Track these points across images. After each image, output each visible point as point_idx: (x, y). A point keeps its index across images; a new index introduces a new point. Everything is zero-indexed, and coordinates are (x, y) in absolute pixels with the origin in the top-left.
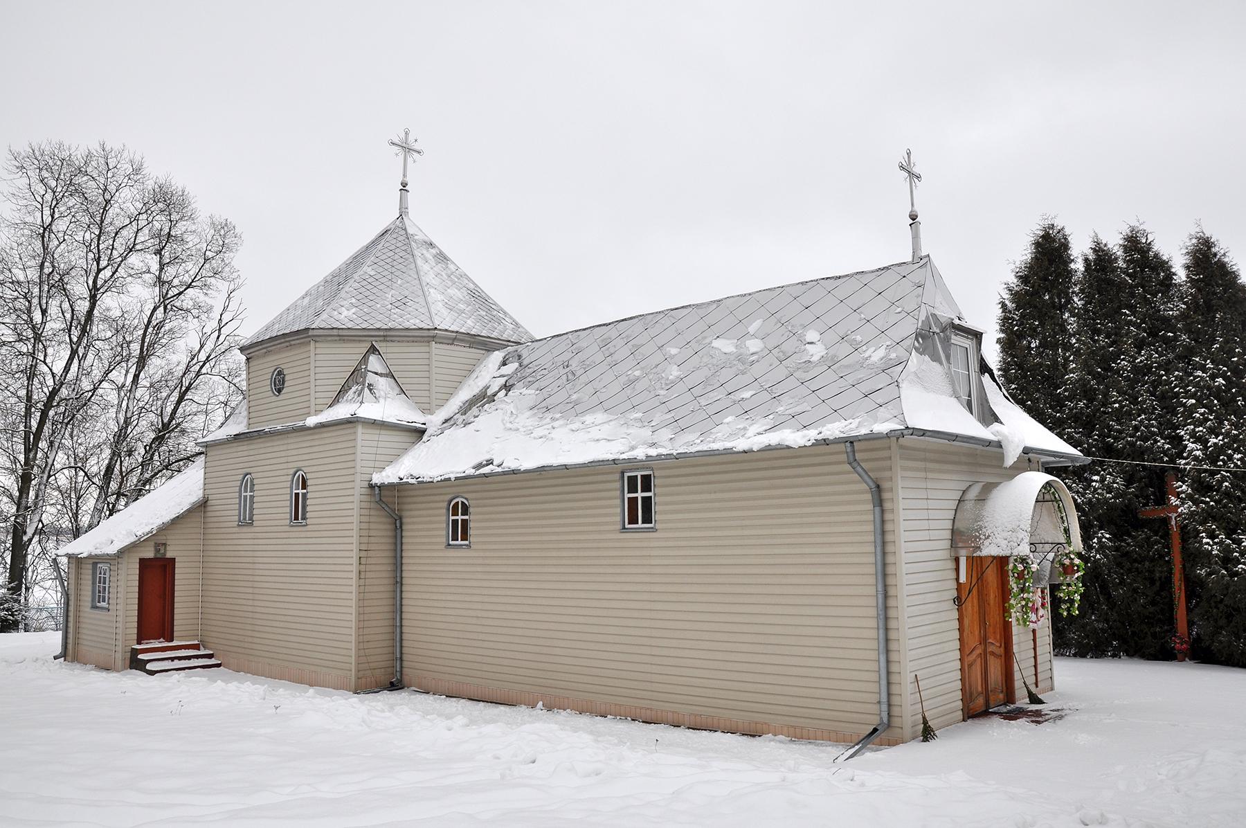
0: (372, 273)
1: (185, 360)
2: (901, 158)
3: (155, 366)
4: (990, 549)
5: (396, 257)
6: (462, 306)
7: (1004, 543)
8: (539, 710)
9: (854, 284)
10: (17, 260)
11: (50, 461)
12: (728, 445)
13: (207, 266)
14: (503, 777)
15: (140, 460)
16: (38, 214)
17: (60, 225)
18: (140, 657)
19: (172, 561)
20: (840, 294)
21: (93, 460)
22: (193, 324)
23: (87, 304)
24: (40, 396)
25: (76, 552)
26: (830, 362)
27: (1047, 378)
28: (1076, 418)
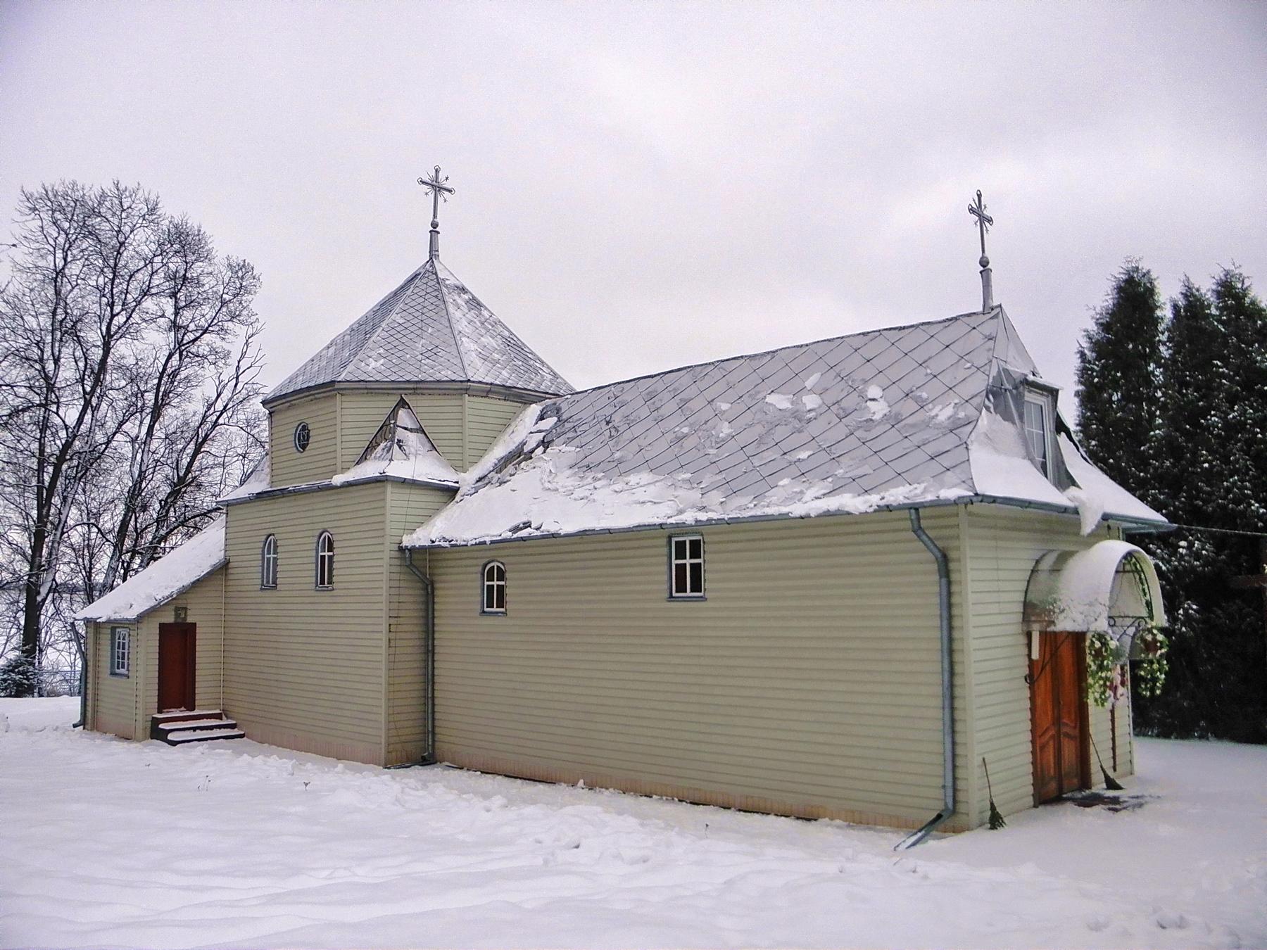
0: (401, 321)
1: (201, 410)
2: (971, 199)
3: (171, 415)
4: (1064, 624)
5: (427, 303)
6: (497, 356)
7: (1080, 618)
8: (580, 791)
9: (920, 336)
10: (29, 306)
11: (63, 517)
12: (784, 510)
13: (224, 309)
14: (546, 862)
15: (155, 516)
16: (51, 258)
17: (74, 269)
18: (161, 726)
20: (906, 345)
21: (106, 517)
22: (210, 371)
23: (101, 352)
24: (53, 447)
25: (95, 616)
26: (894, 420)
27: (1128, 434)
28: (1161, 479)
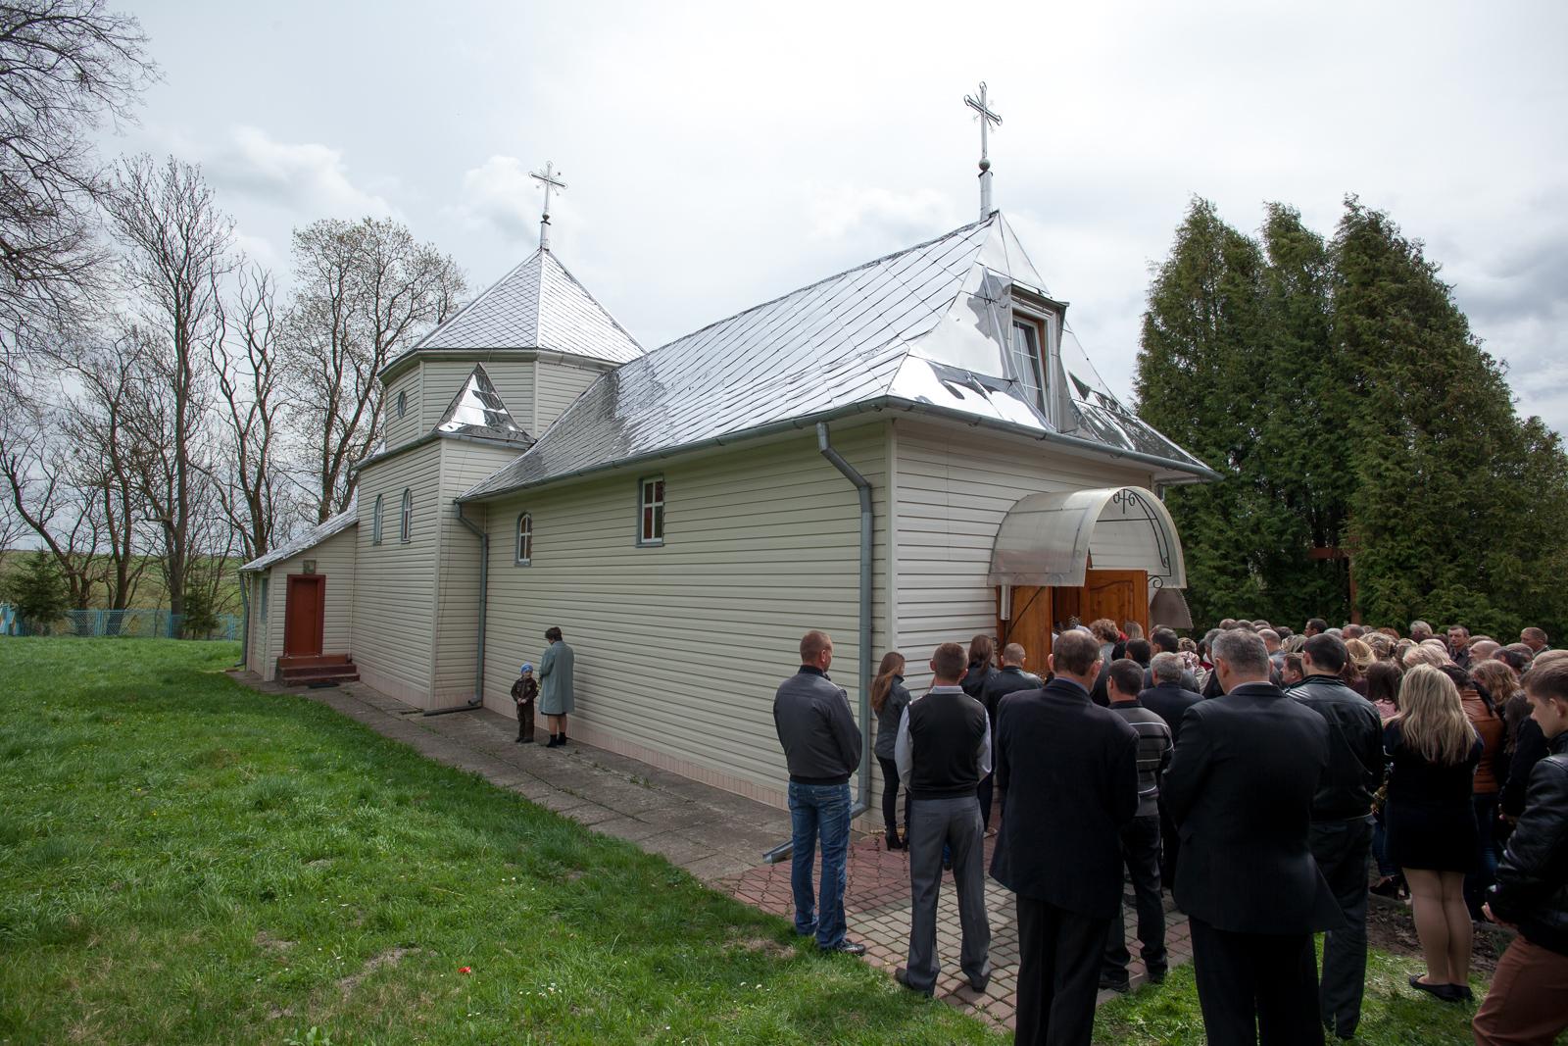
19: (323, 578)
